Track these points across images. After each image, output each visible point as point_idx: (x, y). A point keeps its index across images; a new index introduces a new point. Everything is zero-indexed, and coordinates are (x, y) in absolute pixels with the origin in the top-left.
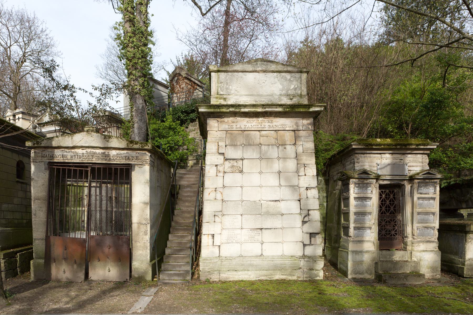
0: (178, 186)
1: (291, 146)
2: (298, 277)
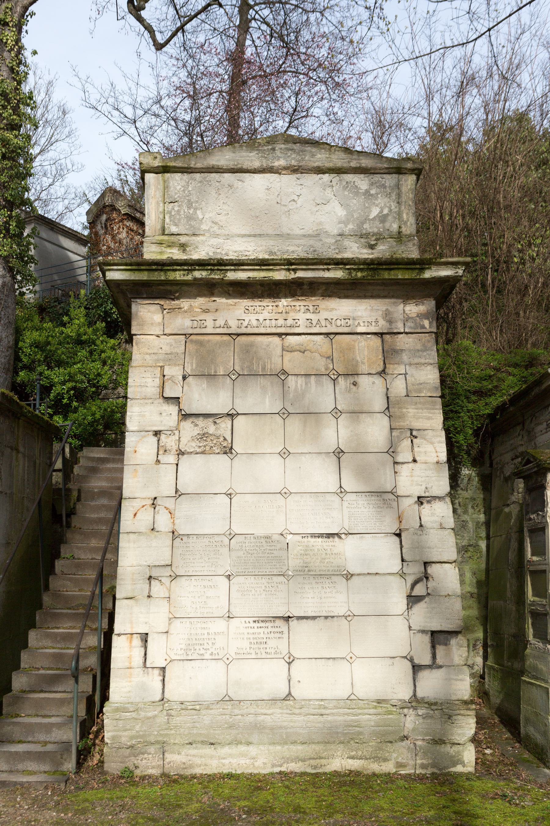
0: (75, 494)
1: (371, 379)
2: (400, 765)
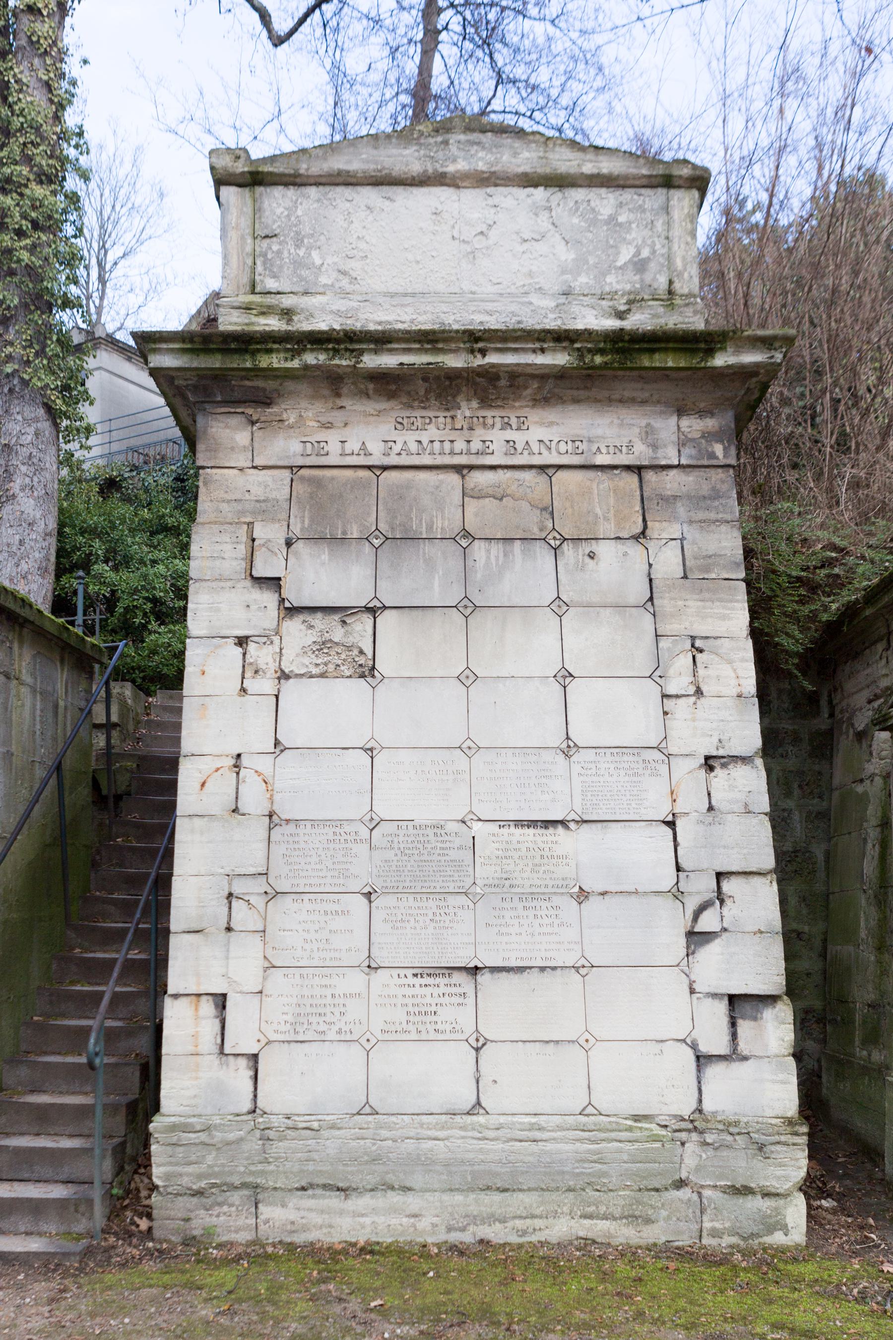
1: (621, 547)
